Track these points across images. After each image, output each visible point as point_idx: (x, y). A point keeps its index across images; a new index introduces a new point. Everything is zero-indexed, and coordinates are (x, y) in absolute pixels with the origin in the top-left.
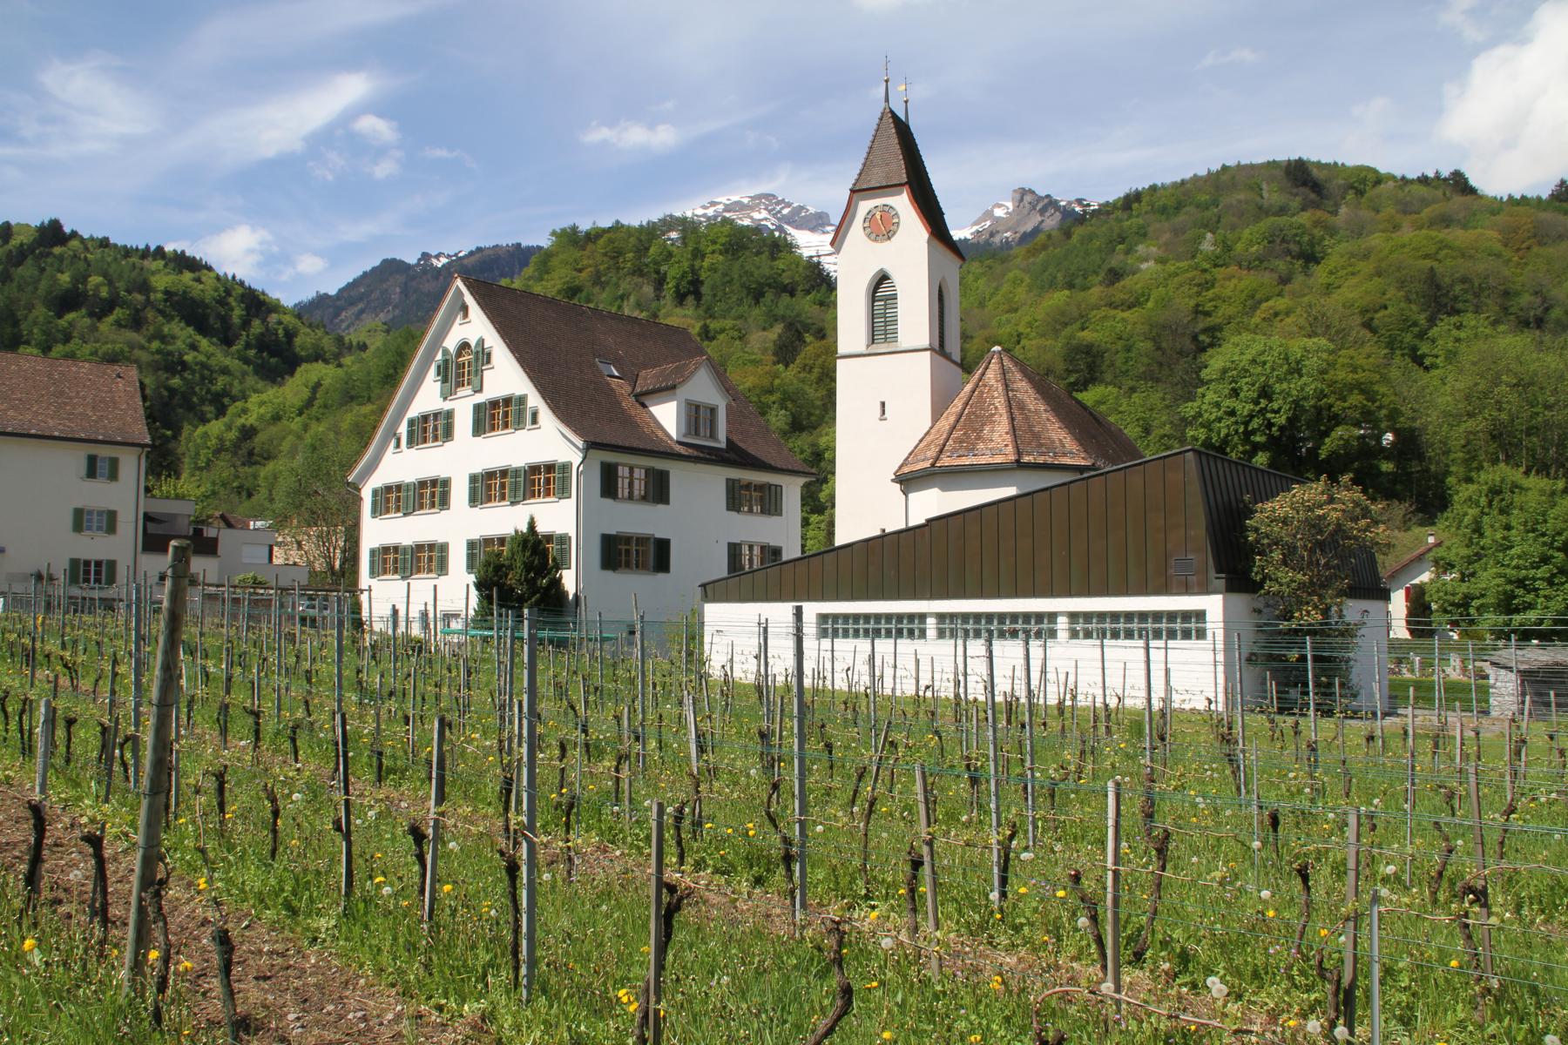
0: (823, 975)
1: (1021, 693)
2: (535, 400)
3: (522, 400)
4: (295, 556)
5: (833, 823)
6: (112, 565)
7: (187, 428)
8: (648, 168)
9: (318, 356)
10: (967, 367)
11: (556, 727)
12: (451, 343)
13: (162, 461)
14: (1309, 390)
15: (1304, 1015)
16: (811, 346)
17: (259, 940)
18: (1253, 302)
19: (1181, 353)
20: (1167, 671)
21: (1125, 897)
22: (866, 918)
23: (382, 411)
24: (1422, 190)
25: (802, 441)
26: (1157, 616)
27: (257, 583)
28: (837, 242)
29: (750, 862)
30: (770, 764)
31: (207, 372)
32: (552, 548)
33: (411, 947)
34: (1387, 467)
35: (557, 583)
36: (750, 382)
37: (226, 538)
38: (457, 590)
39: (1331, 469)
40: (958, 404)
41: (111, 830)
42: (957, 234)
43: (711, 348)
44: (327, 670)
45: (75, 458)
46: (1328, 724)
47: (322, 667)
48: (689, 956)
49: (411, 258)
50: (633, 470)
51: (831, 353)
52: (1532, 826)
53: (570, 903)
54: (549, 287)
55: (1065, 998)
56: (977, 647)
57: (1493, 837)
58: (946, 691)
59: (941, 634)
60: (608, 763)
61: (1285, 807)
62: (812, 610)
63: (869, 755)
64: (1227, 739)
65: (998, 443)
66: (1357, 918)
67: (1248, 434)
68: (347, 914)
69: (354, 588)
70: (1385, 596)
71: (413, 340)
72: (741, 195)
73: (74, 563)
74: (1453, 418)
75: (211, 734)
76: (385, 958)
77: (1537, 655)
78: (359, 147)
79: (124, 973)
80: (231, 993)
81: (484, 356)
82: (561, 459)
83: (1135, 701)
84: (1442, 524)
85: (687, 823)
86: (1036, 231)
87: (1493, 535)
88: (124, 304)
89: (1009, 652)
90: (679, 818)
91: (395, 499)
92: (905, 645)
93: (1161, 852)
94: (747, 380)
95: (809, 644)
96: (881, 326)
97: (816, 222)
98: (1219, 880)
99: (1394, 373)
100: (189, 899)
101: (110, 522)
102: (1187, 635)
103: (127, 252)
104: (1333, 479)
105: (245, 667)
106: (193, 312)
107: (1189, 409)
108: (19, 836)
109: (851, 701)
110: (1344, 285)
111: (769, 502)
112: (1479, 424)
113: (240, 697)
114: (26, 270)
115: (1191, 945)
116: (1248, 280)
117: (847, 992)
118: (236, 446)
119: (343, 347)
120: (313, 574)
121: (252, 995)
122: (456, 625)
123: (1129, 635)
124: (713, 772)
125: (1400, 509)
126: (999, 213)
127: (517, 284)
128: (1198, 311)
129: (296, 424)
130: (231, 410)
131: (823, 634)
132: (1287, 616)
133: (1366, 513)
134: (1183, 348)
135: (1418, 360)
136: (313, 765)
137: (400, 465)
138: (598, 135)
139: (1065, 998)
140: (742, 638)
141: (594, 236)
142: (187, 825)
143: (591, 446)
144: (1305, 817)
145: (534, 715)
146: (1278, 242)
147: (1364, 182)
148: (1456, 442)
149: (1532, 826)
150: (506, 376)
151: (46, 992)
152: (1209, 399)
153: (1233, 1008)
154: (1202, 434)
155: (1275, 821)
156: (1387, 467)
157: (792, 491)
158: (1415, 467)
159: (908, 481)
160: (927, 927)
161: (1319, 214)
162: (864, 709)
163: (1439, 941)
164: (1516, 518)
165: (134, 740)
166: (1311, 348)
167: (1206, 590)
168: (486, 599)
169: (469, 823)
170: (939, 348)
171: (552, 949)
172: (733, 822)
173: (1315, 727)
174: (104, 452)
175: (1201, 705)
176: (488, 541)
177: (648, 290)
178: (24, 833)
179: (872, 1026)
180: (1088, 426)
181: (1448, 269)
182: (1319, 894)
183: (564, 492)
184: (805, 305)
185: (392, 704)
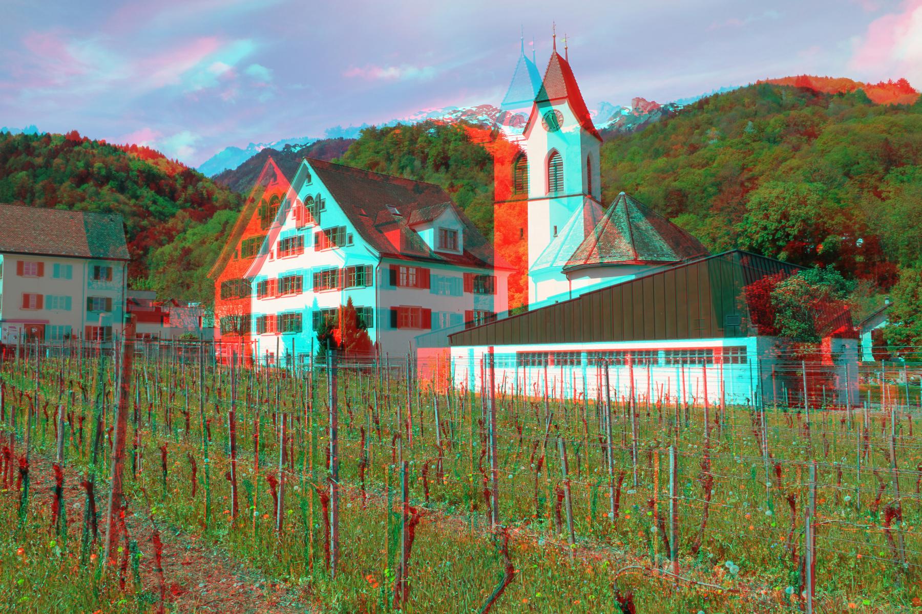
19: (735, 194)
32: (363, 316)
34: (859, 259)
35: (365, 335)
39: (824, 260)
67: (774, 241)
69: (247, 341)
104: (823, 267)
106: (151, 179)
115: (725, 543)
122: (308, 361)
127: (341, 161)
133: (843, 287)
155: (778, 471)
166: (811, 190)
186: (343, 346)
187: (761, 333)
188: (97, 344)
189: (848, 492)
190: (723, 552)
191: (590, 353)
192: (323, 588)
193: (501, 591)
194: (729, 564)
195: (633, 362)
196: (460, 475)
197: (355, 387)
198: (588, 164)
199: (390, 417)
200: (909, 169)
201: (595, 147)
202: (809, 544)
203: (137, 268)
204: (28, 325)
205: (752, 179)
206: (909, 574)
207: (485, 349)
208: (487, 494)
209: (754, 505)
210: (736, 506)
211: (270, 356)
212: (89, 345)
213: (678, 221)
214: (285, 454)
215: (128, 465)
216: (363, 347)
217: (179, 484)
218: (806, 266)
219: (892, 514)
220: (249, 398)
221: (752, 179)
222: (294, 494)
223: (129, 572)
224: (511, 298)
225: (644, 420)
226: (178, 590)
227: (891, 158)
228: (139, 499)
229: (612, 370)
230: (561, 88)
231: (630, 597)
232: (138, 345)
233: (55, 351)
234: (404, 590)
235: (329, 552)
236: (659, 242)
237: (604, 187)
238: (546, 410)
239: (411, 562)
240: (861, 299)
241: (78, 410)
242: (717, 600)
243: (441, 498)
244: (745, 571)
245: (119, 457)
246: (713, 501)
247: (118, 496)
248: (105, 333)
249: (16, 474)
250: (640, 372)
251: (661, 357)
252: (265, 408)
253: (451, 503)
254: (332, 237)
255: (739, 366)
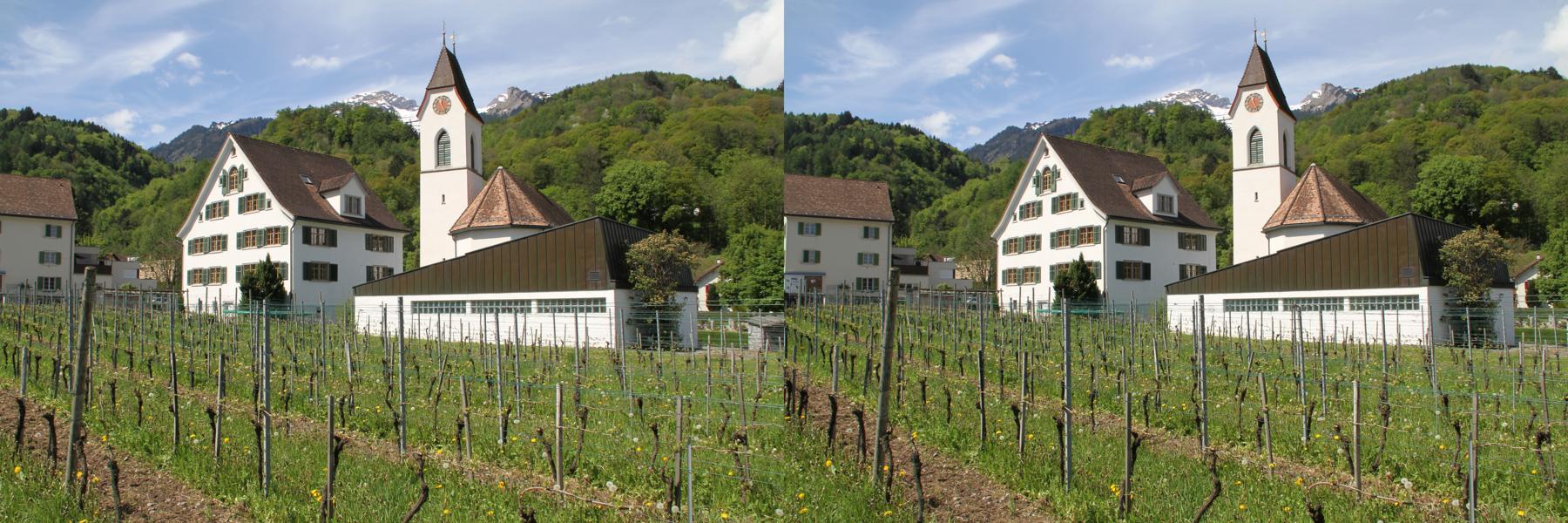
0: (413, 482)
1: (513, 340)
2: (269, 195)
3: (263, 195)
4: (966, 275)
5: (419, 405)
6: (59, 279)
7: (96, 212)
8: (1139, 78)
9: (976, 175)
10: (485, 177)
11: (280, 358)
12: (227, 167)
13: (83, 228)
14: (1475, 182)
15: (655, 500)
16: (408, 166)
17: (132, 467)
18: (1445, 138)
19: (593, 169)
20: (1398, 327)
21: (565, 442)
22: (436, 453)
23: (193, 202)
24: (713, 86)
25: (403, 215)
26: (581, 301)
27: (131, 288)
28: (420, 115)
29: (378, 426)
30: (388, 376)
31: (106, 183)
32: (279, 269)
33: (209, 470)
34: (696, 225)
35: (1094, 286)
36: (1191, 184)
37: (116, 266)
38: (231, 291)
39: (668, 227)
40: (481, 196)
41: (58, 411)
42: (1292, 108)
43: (357, 169)
44: (166, 331)
45: (858, 228)
46: (667, 354)
47: (164, 330)
48: (347, 473)
49: (207, 125)
50: (1131, 230)
51: (417, 170)
52: (770, 405)
53: (288, 447)
54: (1089, 139)
55: (536, 492)
56: (491, 317)
57: (750, 411)
58: (476, 339)
59: (473, 311)
60: (307, 376)
61: (645, 396)
62: (408, 299)
63: (437, 372)
64: (617, 362)
65: (1314, 212)
66: (681, 451)
67: (1442, 206)
68: (177, 453)
69: (179, 290)
70: (696, 290)
71: (208, 166)
72: (372, 92)
73: (40, 279)
74: (1550, 195)
75: (109, 364)
76: (196, 475)
77: (772, 319)
78: (998, 71)
79: (872, 479)
80: (117, 493)
81: (244, 174)
82: (283, 225)
83: (571, 344)
84: (724, 254)
85: (346, 406)
86: (520, 108)
87: (749, 259)
88: (64, 149)
89: (506, 320)
90: (342, 403)
91: (200, 246)
92: (455, 317)
93: (584, 419)
94: (375, 185)
95: (407, 316)
96: (442, 157)
97: (409, 105)
98: (614, 432)
99: (700, 178)
100: (96, 446)
101: (58, 258)
102: (596, 310)
103: (65, 123)
104: (669, 231)
105: (126, 331)
106: (914, 155)
107: (597, 197)
108: (13, 416)
109: (428, 345)
110: (1492, 128)
111: (387, 246)
112: (742, 203)
113: (123, 345)
114: (14, 133)
115: (1401, 463)
116: (627, 132)
117: (426, 490)
118: (121, 220)
119: (989, 170)
120: (159, 283)
121: (129, 494)
122: (231, 308)
123: (567, 310)
124: (360, 381)
125: (703, 246)
126: (501, 99)
127: (260, 137)
128: (1417, 143)
129: (150, 208)
130: (935, 202)
131: (414, 311)
132: (647, 300)
133: (686, 248)
134: (1409, 162)
135: (1531, 166)
136: (159, 378)
137: (202, 228)
138: (1115, 61)
139: (536, 492)
140: (373, 313)
141: (298, 113)
142: (96, 409)
143: (1110, 217)
144: (656, 401)
145: (269, 351)
146: (1457, 107)
147: (684, 82)
148: (731, 213)
149: (770, 405)
150: (1068, 184)
151: (26, 493)
152: (1422, 189)
153: (619, 497)
154: (604, 210)
155: (1446, 401)
156: (696, 225)
157: (1211, 238)
158: (1530, 220)
159: (456, 234)
160: (467, 457)
161: (662, 99)
162: (436, 349)
163: (723, 463)
164: (761, 250)
165: (70, 367)
166: (1476, 161)
167: (606, 288)
168: (246, 295)
169: (237, 407)
170: (1284, 165)
171: (279, 469)
172: (369, 406)
173: (660, 356)
174: (54, 223)
175: (604, 345)
176: (246, 266)
177: (326, 140)
178: (16, 414)
179: (439, 507)
180: (546, 206)
181: (726, 125)
182: (663, 440)
183: (1097, 241)
184: (404, 147)
185: (199, 348)
186: (1077, 295)
187: (1431, 283)
188: (867, 293)
189: (1505, 419)
190: (1398, 471)
191: (1285, 300)
192: (1059, 501)
193: (1210, 504)
194: (1404, 480)
195: (1322, 308)
196: (1176, 404)
197: (1087, 329)
198: (471, 143)
199: (1116, 355)
200: (1558, 144)
201: (1290, 123)
202: (1472, 462)
203: (83, 228)
204: (808, 277)
205: (1424, 153)
206: (1558, 489)
207: (1196, 297)
208: (1198, 420)
209: (1425, 431)
210: (1410, 431)
211: (1014, 304)
212: (40, 293)
213: (1361, 188)
214: (1026, 387)
215: (893, 396)
216: (1093, 296)
217: (937, 411)
218: (1470, 226)
219: (1543, 438)
220: (996, 340)
221: (1424, 153)
222: (1033, 421)
223: (894, 487)
224: (1219, 254)
225: (1332, 357)
226: (934, 503)
227: (1542, 134)
228: (902, 425)
229: (1305, 314)
230: (450, 78)
231: (1320, 509)
232: (902, 294)
233: (831, 299)
234: (1127, 503)
235: (1064, 469)
236: (1344, 207)
237: (1298, 159)
238: (1247, 349)
239: (1133, 479)
240: (1518, 255)
241: (850, 350)
242: (1393, 511)
243: (1158, 425)
244: (1418, 487)
245: (886, 388)
246: (1391, 427)
247: (884, 421)
248: (871, 284)
249: (798, 404)
250: (1328, 316)
251: (1281, 304)
252: (1009, 347)
253: (1168, 429)
254: (251, 203)
255: (1412, 311)
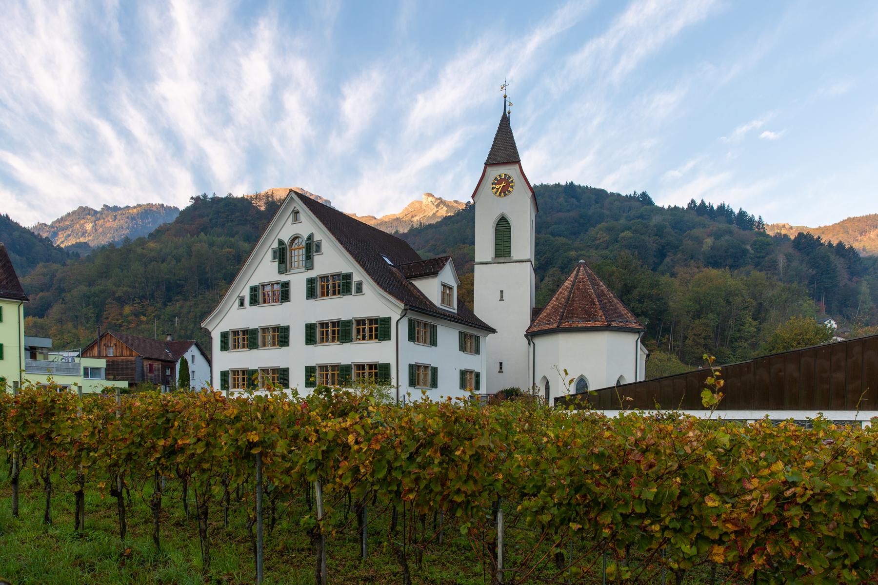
2: (358, 275)
3: (348, 276)
96: (503, 250)
